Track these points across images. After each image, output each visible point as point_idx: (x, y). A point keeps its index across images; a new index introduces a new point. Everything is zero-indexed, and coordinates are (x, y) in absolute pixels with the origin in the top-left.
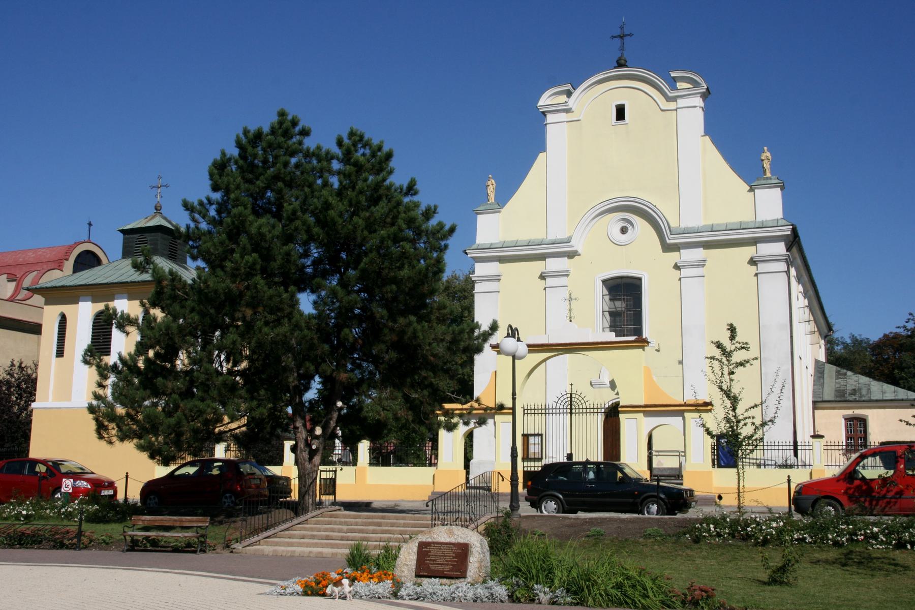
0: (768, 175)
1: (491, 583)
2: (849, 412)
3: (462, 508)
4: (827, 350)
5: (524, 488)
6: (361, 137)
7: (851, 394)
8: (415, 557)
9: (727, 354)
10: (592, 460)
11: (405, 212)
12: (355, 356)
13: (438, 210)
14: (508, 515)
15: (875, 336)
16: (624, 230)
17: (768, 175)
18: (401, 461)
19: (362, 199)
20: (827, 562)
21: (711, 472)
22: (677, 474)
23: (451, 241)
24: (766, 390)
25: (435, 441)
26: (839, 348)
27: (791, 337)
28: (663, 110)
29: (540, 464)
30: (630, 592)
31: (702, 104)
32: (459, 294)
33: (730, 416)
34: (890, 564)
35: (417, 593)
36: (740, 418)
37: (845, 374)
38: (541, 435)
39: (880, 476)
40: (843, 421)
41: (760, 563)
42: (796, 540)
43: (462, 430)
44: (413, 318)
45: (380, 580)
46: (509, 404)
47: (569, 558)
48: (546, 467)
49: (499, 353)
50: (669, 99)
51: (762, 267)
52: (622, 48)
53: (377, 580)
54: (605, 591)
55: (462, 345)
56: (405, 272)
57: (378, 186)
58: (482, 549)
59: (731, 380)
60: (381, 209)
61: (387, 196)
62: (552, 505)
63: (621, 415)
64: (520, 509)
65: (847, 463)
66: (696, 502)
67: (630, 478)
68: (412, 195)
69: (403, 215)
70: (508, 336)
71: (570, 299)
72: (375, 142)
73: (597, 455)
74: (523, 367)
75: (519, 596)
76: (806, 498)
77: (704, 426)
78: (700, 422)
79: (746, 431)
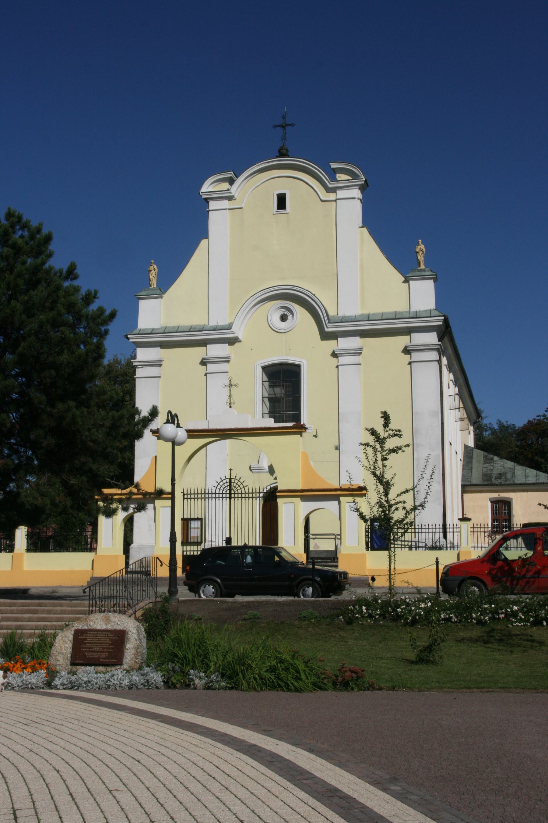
0: (422, 267)
1: (147, 670)
2: (495, 495)
3: (120, 593)
4: (475, 435)
5: (183, 572)
6: (20, 218)
7: (497, 478)
8: (71, 645)
9: (381, 441)
10: (250, 544)
11: (64, 297)
12: (12, 441)
13: (98, 295)
14: (166, 600)
15: (520, 422)
16: (284, 318)
17: (422, 267)
18: (61, 546)
19: (21, 282)
20: (471, 640)
21: (364, 555)
22: (332, 557)
23: (112, 327)
24: (417, 474)
25: (95, 525)
26: (487, 433)
27: (442, 423)
28: (322, 201)
29: (199, 548)
30: (283, 674)
31: (360, 196)
32: (120, 378)
33: (383, 501)
34: (528, 640)
35: (71, 682)
36: (392, 502)
37: (492, 459)
38: (201, 519)
39: (520, 557)
40: (489, 504)
41: (408, 643)
42: (443, 620)
43: (121, 515)
44: (72, 404)
45: (34, 670)
46: (168, 489)
47: (227, 643)
48: (204, 551)
49: (159, 438)
50: (329, 190)
51: (416, 356)
52: (284, 138)
53: (30, 670)
54: (259, 674)
55: (122, 430)
56: (65, 357)
57: (37, 269)
58: (138, 635)
59: (384, 466)
60: (39, 293)
61: (46, 279)
62: (211, 589)
63: (279, 501)
64: (179, 594)
65: (492, 545)
66: (350, 584)
67: (286, 561)
68: (72, 279)
69: (63, 300)
70: (168, 422)
71: (230, 385)
72: (34, 224)
73: (256, 540)
74: (182, 453)
75: (175, 681)
76: (454, 579)
77: (357, 510)
78: (354, 507)
79: (397, 515)
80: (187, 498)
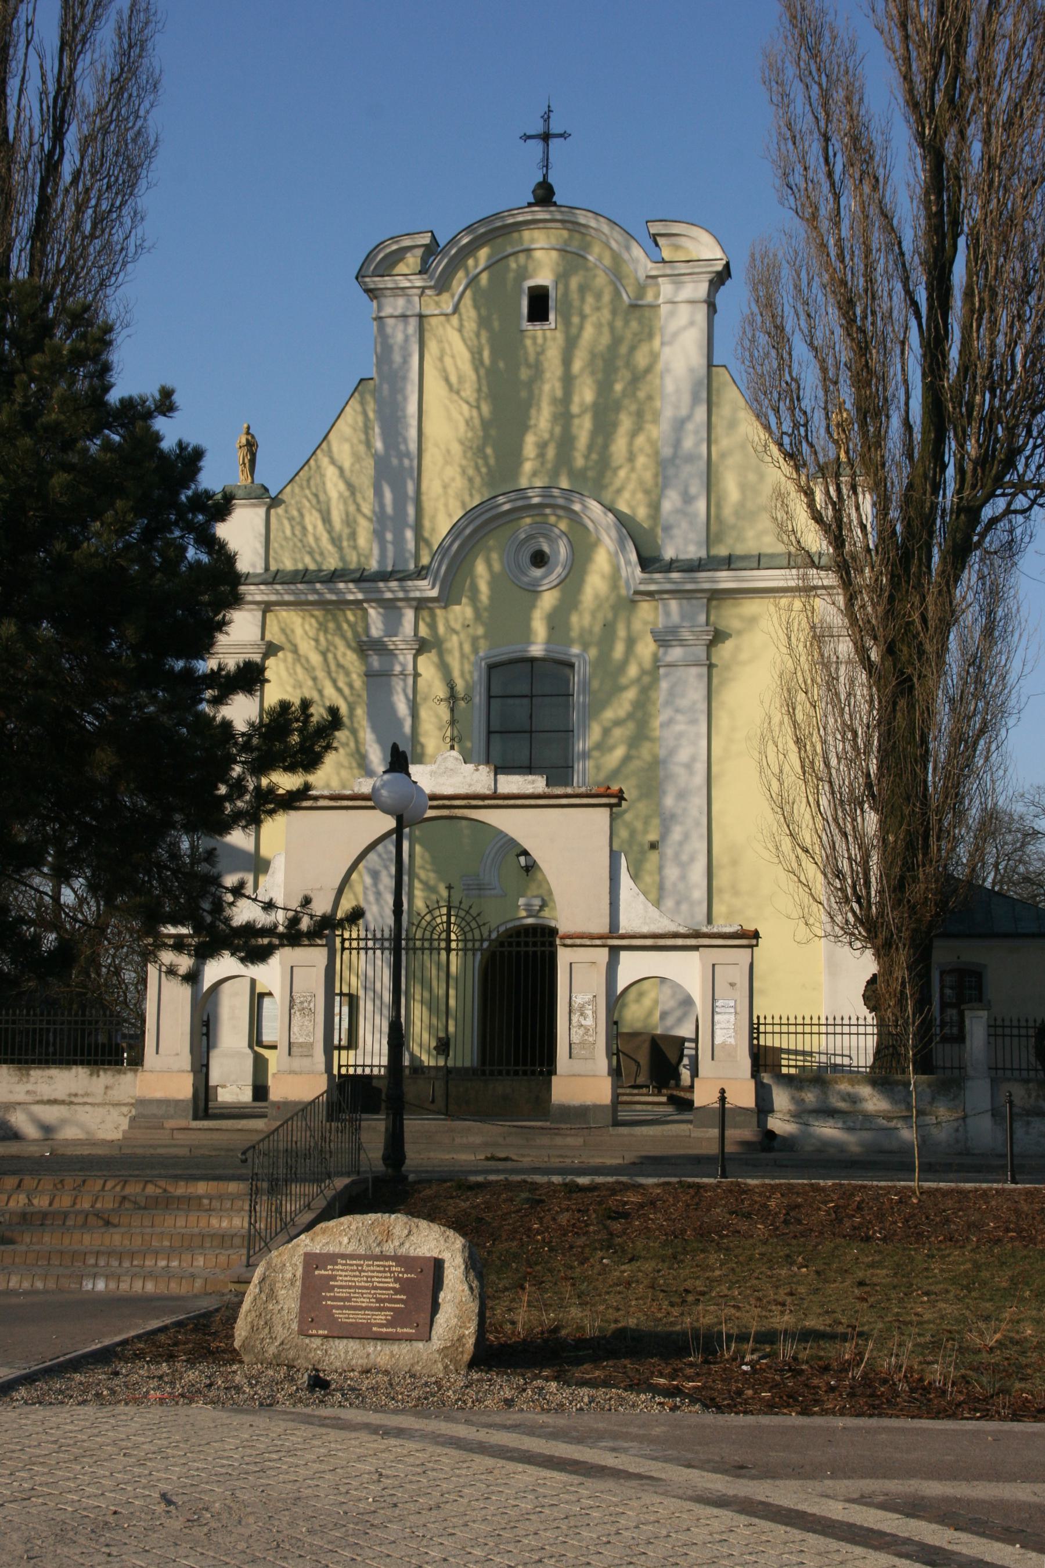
80: (351, 949)
